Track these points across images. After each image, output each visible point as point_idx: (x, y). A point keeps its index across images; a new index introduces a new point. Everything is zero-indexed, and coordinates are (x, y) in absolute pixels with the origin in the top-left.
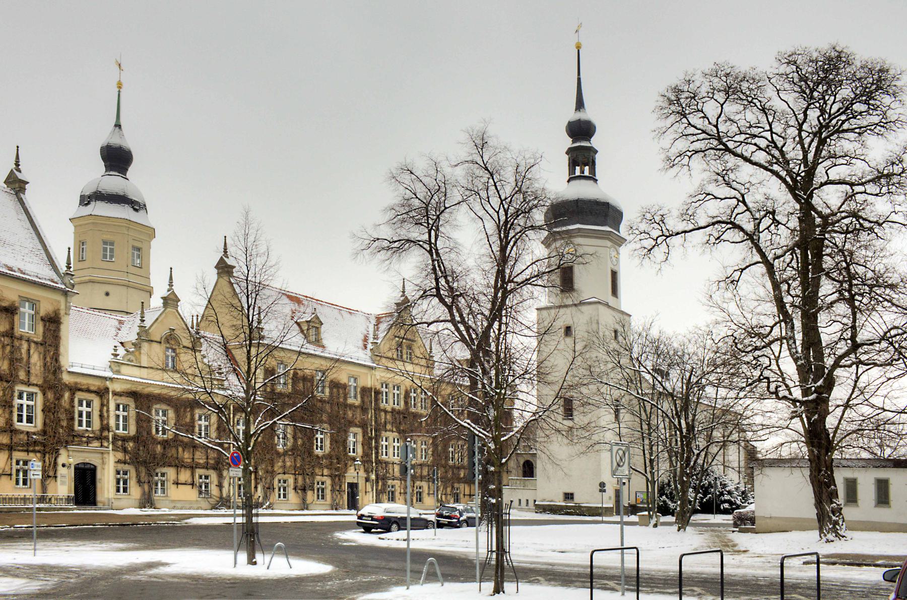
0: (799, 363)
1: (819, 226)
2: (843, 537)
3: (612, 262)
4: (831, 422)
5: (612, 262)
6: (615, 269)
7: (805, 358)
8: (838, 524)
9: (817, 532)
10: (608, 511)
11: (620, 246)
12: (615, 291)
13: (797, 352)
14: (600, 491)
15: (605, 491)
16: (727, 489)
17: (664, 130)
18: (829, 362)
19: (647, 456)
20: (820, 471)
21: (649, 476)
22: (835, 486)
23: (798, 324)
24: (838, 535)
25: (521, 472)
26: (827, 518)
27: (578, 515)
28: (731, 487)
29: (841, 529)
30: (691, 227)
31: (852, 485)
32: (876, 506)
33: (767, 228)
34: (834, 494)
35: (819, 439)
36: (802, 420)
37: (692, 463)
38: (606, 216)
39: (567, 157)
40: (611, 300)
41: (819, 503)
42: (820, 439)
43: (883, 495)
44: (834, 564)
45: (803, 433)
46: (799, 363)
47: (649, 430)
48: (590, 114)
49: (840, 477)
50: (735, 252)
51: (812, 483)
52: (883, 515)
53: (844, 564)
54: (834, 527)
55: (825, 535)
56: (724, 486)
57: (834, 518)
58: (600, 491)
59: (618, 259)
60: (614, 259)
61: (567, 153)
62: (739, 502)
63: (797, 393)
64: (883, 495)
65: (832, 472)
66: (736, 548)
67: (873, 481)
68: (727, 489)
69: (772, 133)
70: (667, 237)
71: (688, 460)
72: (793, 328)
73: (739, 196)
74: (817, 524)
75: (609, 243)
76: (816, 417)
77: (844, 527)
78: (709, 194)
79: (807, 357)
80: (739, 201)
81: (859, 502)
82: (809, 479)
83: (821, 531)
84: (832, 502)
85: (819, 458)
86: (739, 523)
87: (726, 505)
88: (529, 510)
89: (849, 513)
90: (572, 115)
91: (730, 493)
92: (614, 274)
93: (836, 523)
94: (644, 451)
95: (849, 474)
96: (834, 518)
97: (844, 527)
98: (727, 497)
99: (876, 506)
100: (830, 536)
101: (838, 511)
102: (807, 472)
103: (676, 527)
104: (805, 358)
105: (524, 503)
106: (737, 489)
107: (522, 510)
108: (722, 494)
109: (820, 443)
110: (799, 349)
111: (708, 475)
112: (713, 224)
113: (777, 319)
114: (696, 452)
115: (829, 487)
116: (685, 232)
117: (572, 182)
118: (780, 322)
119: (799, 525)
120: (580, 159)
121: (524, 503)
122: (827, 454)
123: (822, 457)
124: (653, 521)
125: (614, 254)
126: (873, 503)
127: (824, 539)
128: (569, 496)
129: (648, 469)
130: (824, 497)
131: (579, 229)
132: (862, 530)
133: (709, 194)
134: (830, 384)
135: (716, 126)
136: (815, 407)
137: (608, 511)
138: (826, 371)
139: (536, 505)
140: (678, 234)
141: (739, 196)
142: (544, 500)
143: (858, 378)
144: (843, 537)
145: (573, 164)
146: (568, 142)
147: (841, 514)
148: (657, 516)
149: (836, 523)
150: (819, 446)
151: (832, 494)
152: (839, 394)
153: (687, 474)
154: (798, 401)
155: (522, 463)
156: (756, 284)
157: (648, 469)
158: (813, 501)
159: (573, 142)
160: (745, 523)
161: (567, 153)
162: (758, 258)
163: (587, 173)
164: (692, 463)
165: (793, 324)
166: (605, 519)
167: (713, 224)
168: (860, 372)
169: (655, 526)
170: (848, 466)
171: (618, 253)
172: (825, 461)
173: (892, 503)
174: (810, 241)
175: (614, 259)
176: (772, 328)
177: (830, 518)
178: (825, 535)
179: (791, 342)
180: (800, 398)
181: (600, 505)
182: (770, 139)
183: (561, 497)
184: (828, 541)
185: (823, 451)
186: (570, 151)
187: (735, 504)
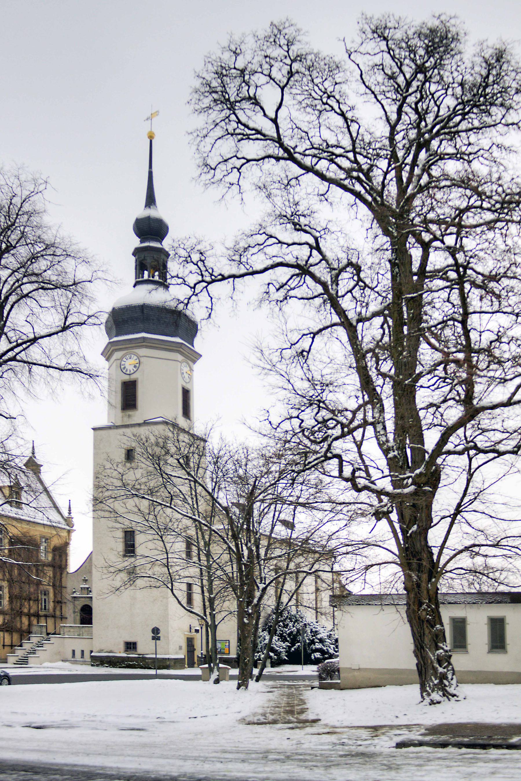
0: (390, 455)
1: (415, 274)
2: (454, 696)
3: (183, 378)
4: (435, 537)
5: (183, 378)
6: (187, 386)
7: (398, 449)
8: (447, 678)
9: (417, 688)
10: (178, 663)
11: (194, 362)
12: (186, 412)
13: (387, 441)
14: (154, 638)
15: (159, 639)
16: (319, 636)
17: (205, 132)
18: (431, 439)
19: (206, 594)
20: (421, 604)
21: (209, 620)
22: (442, 624)
23: (389, 404)
24: (446, 694)
25: (78, 618)
26: (431, 672)
27: (142, 668)
28: (323, 635)
29: (450, 685)
30: (243, 271)
31: (460, 626)
32: (489, 652)
33: (350, 291)
34: (440, 637)
35: (418, 560)
36: (391, 522)
37: (255, 601)
38: (176, 325)
39: (133, 259)
40: (182, 422)
41: (420, 650)
42: (420, 560)
43: (498, 640)
44: (444, 745)
45: (397, 553)
46: (390, 455)
47: (208, 561)
48: (161, 211)
49: (447, 614)
50: (306, 314)
51: (410, 621)
52: (498, 662)
53: (460, 745)
54: (441, 682)
55: (429, 695)
56: (315, 633)
57: (441, 670)
58: (154, 638)
59: (190, 377)
60: (186, 376)
61: (134, 254)
62: (331, 651)
63: (386, 484)
64: (498, 640)
65: (437, 607)
66: (303, 717)
67: (485, 620)
68: (319, 636)
69: (355, 153)
70: (209, 283)
71: (251, 596)
72: (382, 410)
73: (312, 241)
74: (416, 677)
75: (180, 357)
76: (415, 528)
77: (454, 682)
78: (271, 237)
79: (402, 448)
80: (311, 247)
81: (469, 647)
82: (405, 616)
83: (423, 689)
84: (437, 648)
85: (418, 586)
86: (324, 676)
87: (318, 655)
88: (84, 663)
89: (459, 661)
90: (140, 211)
91: (321, 641)
92: (186, 394)
93: (444, 677)
94: (202, 587)
95: (458, 612)
96: (441, 670)
97: (454, 682)
98: (318, 646)
99: (489, 652)
100: (436, 696)
101: (445, 660)
102: (403, 610)
103: (235, 683)
104: (398, 449)
105: (78, 654)
106: (329, 636)
107: (75, 662)
108: (313, 642)
109: (420, 566)
110: (391, 437)
111: (296, 621)
112: (273, 267)
113: (361, 401)
114: (261, 586)
115: (433, 627)
116: (234, 276)
117: (138, 287)
118: (365, 404)
119: (396, 678)
120: (149, 261)
121: (78, 654)
122: (430, 580)
123: (423, 585)
124: (215, 675)
125: (186, 369)
126: (486, 648)
127: (427, 700)
128: (131, 646)
129: (208, 611)
130: (427, 640)
131: (144, 338)
132: (473, 683)
133: (271, 237)
134: (433, 478)
135: (275, 121)
136: (412, 511)
137: (178, 663)
138: (427, 456)
139: (92, 657)
140: (224, 278)
141: (312, 241)
142: (101, 651)
143: (471, 475)
144: (454, 696)
145: (141, 267)
146: (136, 242)
147: (450, 664)
148: (219, 669)
149: (444, 677)
150: (420, 569)
151: (437, 636)
152: (444, 500)
153: (249, 615)
154: (387, 494)
155: (79, 608)
156: (333, 352)
157: (208, 611)
158: (412, 647)
159: (141, 242)
160: (330, 677)
161: (134, 254)
162: (336, 319)
163: (157, 278)
164: (255, 601)
165: (382, 405)
166: (160, 672)
167: (273, 267)
168: (474, 465)
169: (217, 681)
170: (456, 603)
171: (191, 370)
172: (428, 590)
173: (509, 648)
174: (407, 287)
175: (186, 376)
176: (354, 413)
177: (435, 670)
178: (429, 695)
179: (379, 427)
180: (389, 488)
181: (154, 656)
182: (353, 159)
183: (122, 647)
184: (432, 703)
185: (425, 577)
186: (137, 252)
187: (328, 653)
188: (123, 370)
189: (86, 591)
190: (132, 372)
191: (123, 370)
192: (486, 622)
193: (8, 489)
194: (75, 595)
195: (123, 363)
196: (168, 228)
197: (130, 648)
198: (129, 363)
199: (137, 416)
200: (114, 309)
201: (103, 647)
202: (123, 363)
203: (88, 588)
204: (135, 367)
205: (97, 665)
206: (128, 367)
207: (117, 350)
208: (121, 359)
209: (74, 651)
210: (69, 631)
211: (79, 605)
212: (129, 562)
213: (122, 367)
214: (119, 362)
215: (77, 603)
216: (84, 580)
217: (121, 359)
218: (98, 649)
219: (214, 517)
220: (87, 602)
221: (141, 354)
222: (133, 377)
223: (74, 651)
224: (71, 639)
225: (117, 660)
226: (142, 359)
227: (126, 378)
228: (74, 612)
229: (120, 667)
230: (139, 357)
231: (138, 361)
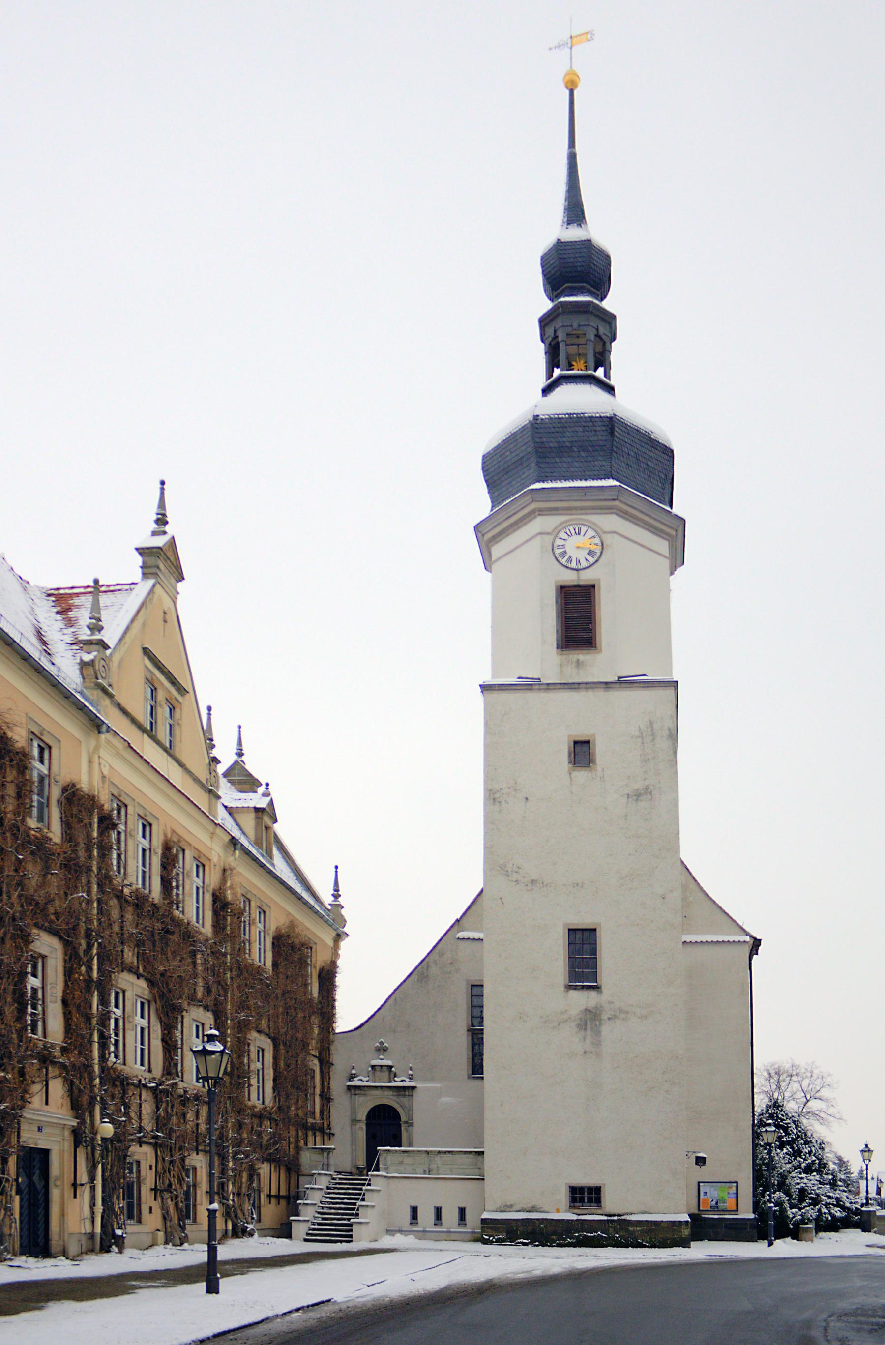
128: (585, 1195)
155: (362, 1115)
183: (564, 1197)
188: (560, 558)
189: (387, 1074)
190: (584, 564)
191: (560, 558)
192: (428, 1288)
193: (252, 815)
194: (356, 1082)
195: (559, 542)
196: (608, 257)
197: (582, 1201)
198: (577, 546)
199: (597, 665)
200: (536, 417)
201: (510, 1199)
202: (559, 542)
203: (391, 1067)
204: (591, 553)
205: (500, 1242)
206: (571, 551)
207: (541, 512)
208: (556, 533)
209: (414, 1210)
210: (401, 1163)
211: (365, 1105)
212: (581, 1000)
213: (557, 551)
214: (548, 539)
215: (359, 1100)
216: (378, 1050)
217: (556, 533)
218: (499, 1203)
219: (103, 987)
220: (389, 1099)
221: (607, 528)
222: (586, 577)
223: (414, 1210)
224: (406, 1181)
225: (551, 1229)
226: (608, 539)
227: (570, 578)
228: (354, 1121)
229: (559, 1245)
230: (599, 533)
231: (597, 540)
